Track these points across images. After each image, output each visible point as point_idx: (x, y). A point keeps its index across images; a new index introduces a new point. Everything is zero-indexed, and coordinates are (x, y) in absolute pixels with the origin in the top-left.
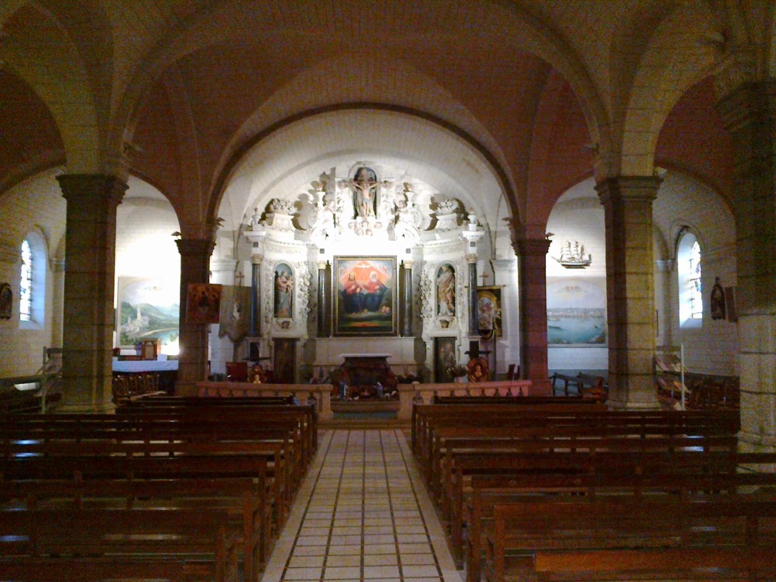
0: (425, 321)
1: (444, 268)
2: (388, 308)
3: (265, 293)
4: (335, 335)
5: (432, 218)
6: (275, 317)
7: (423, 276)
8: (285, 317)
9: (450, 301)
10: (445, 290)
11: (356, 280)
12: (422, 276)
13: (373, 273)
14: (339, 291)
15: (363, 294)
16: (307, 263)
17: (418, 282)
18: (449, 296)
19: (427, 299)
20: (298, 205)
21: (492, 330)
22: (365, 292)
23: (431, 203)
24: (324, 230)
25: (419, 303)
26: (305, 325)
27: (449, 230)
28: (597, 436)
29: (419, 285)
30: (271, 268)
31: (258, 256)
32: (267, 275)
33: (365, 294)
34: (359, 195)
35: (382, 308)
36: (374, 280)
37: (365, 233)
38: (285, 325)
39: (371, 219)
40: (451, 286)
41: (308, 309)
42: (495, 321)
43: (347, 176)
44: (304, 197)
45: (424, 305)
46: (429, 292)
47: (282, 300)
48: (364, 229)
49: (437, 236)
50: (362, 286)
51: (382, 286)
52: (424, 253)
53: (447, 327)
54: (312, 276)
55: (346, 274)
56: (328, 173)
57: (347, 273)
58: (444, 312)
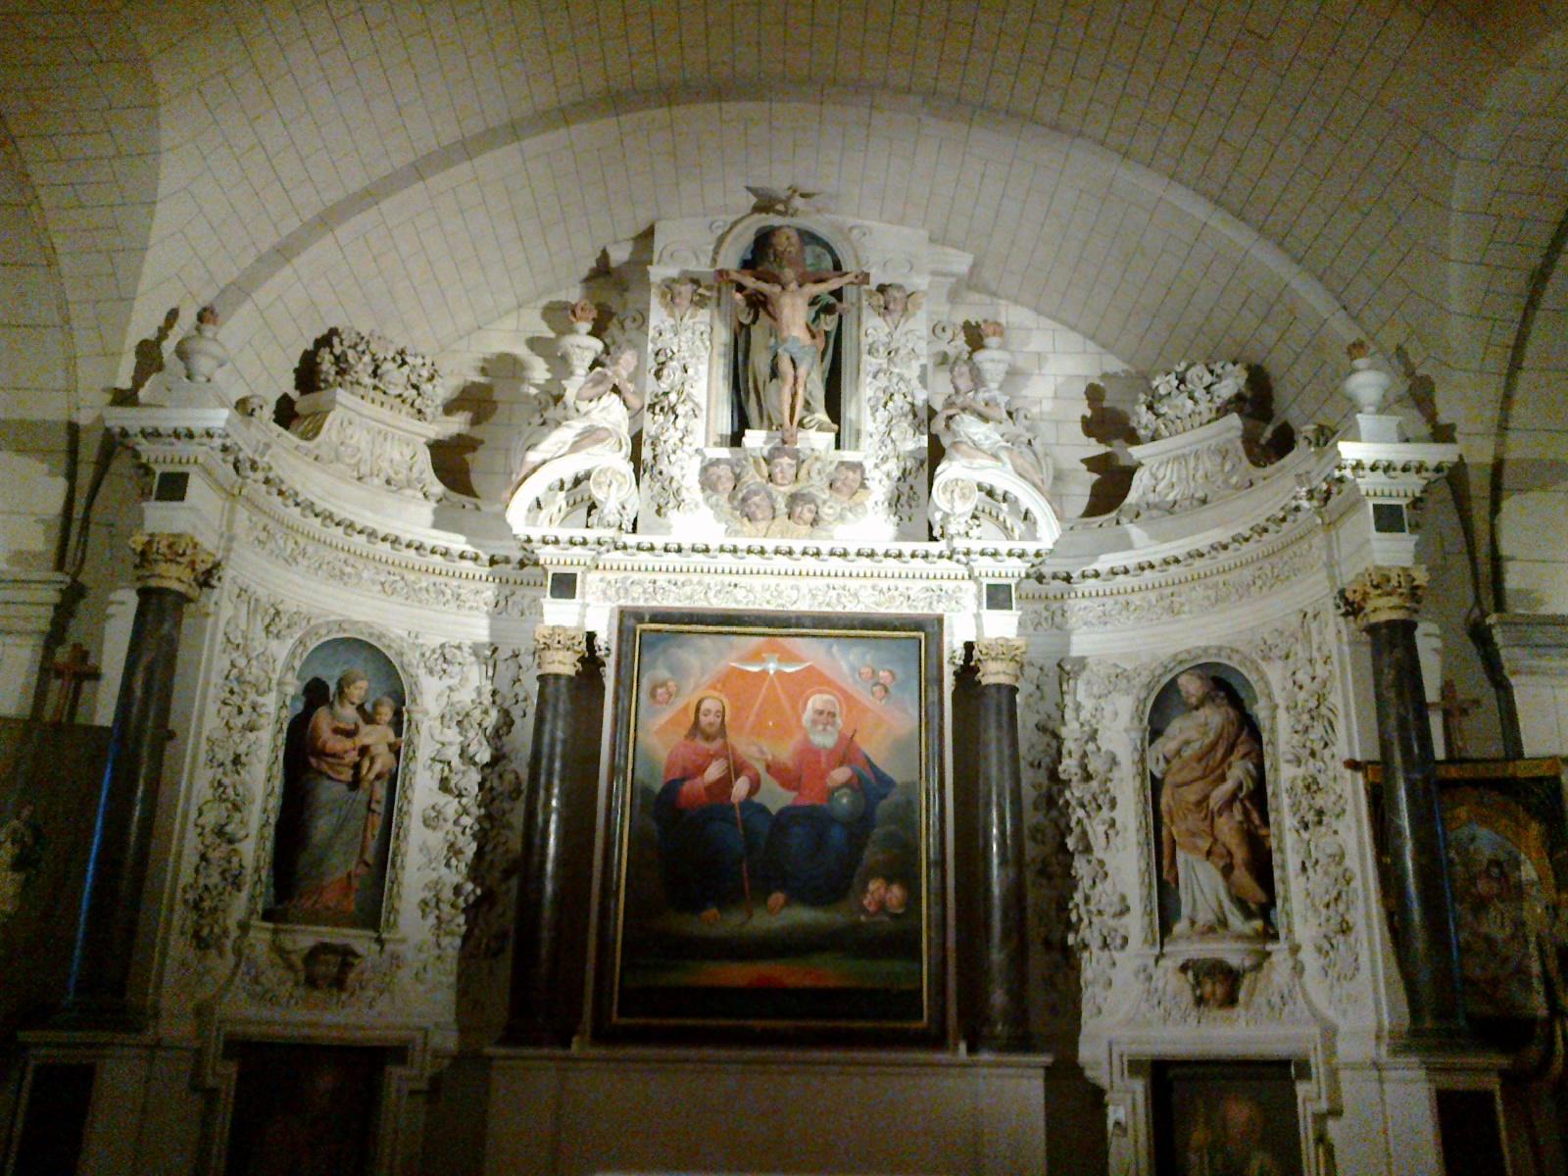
0: (1092, 967)
1: (1191, 686)
2: (896, 893)
3: (204, 778)
4: (605, 1035)
5: (1096, 477)
6: (267, 916)
7: (1070, 731)
8: (337, 919)
9: (1240, 855)
10: (1206, 797)
11: (732, 738)
12: (1064, 732)
13: (816, 701)
14: (641, 792)
15: (762, 809)
16: (490, 655)
17: (1046, 761)
18: (1228, 829)
19: (1098, 853)
20: (475, 401)
21: (1549, 1023)
22: (776, 797)
23: (1088, 413)
24: (577, 482)
25: (1056, 869)
26: (446, 974)
27: (1204, 501)
28: (94, 876)
29: (1053, 775)
30: (281, 650)
31: (177, 549)
32: (237, 683)
33: (774, 809)
34: (758, 334)
35: (864, 889)
36: (825, 740)
37: (781, 506)
38: (329, 966)
39: (817, 440)
40: (1238, 771)
41: (469, 886)
42: (1553, 964)
43: (706, 260)
44: (507, 367)
45: (1085, 884)
46: (1105, 813)
47: (322, 826)
48: (781, 492)
49: (1135, 531)
50: (761, 768)
51: (868, 774)
52: (1073, 621)
53: (1230, 1000)
54: (507, 721)
55: (679, 703)
56: (619, 255)
57: (688, 698)
58: (1205, 916)
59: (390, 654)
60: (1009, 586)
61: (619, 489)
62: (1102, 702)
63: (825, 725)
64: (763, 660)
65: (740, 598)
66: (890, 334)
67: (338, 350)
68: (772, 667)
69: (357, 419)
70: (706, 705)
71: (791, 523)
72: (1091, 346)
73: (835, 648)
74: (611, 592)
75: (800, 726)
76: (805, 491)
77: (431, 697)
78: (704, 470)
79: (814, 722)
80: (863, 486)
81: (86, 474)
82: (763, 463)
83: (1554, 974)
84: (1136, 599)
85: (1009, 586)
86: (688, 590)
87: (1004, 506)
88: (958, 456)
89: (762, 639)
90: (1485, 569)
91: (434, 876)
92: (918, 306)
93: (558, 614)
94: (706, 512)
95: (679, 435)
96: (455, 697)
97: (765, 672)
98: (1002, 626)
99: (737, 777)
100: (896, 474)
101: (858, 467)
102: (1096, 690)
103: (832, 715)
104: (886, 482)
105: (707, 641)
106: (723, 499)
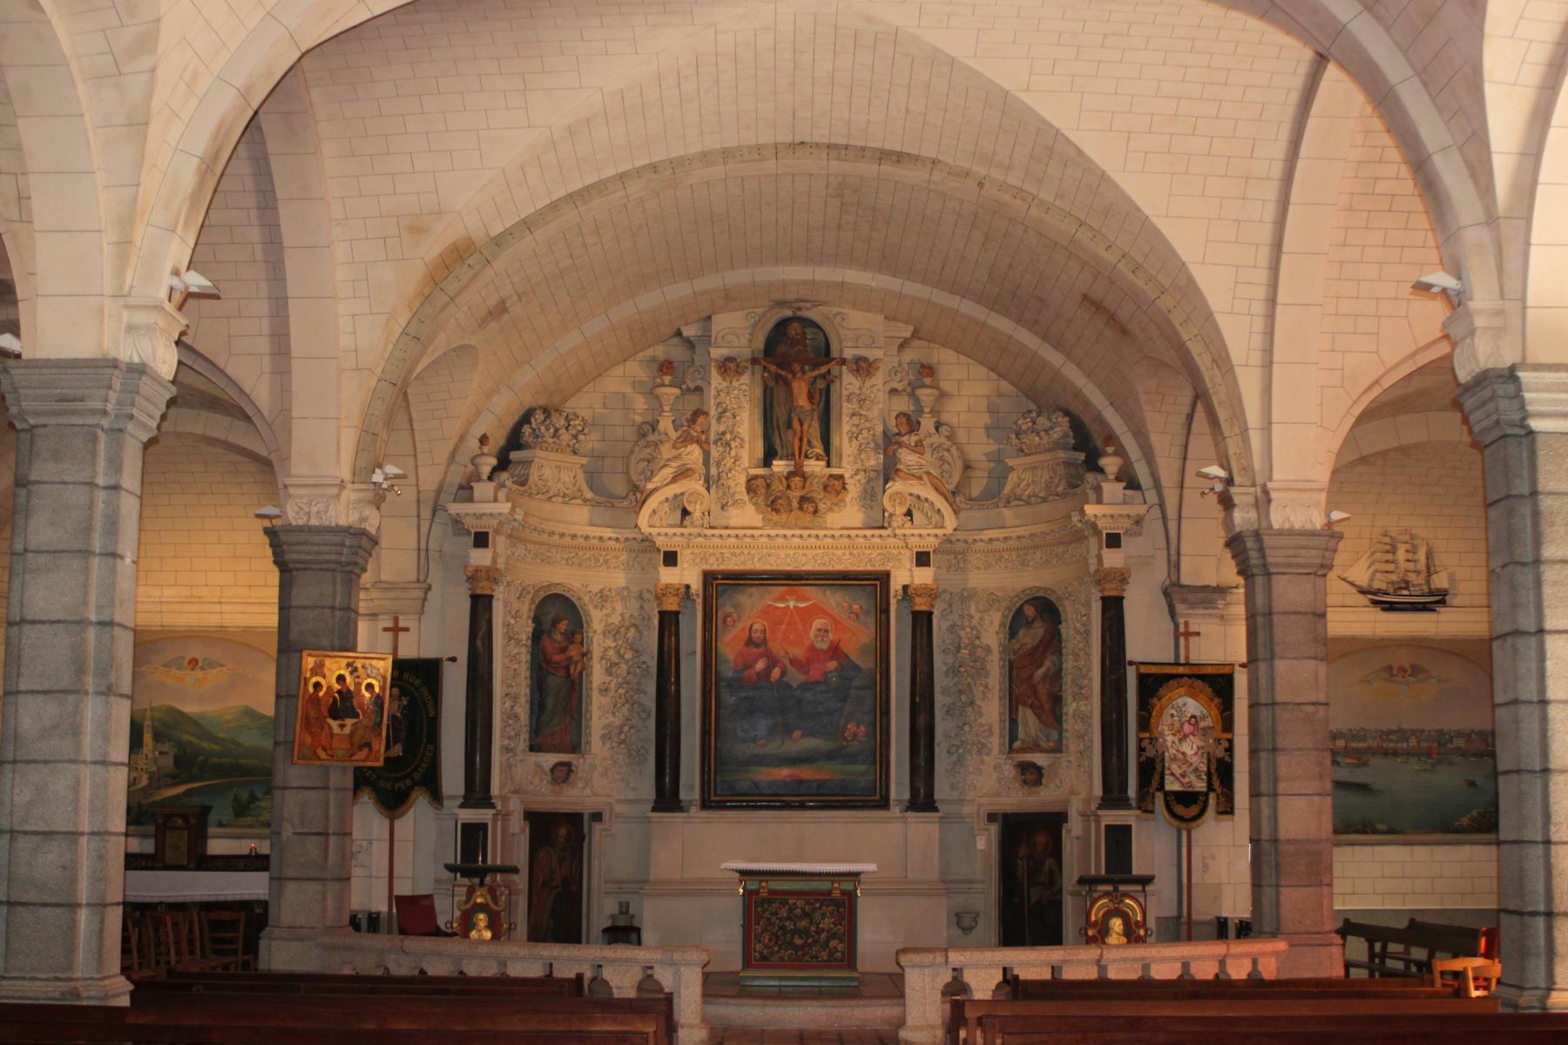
1: (1030, 611)
13: (818, 623)
37: (795, 504)
39: (814, 466)
42: (1213, 767)
43: (744, 341)
48: (795, 495)
50: (787, 662)
59: (574, 600)
60: (929, 553)
61: (701, 504)
62: (984, 614)
63: (822, 637)
64: (786, 600)
65: (772, 562)
66: (860, 388)
67: (534, 426)
68: (792, 604)
69: (545, 463)
70: (755, 627)
71: (800, 513)
72: (993, 376)
73: (828, 592)
74: (698, 561)
75: (809, 638)
76: (809, 496)
77: (597, 620)
78: (749, 481)
79: (817, 636)
80: (844, 488)
81: (424, 529)
82: (784, 480)
83: (1213, 771)
84: (1006, 555)
85: (929, 553)
86: (742, 558)
87: (926, 505)
88: (897, 479)
89: (784, 588)
90: (1174, 558)
91: (607, 722)
92: (877, 369)
93: (669, 576)
94: (750, 508)
95: (733, 460)
96: (610, 620)
97: (788, 607)
98: (924, 576)
99: (774, 667)
100: (863, 481)
101: (841, 477)
102: (981, 608)
103: (826, 631)
104: (858, 484)
105: (754, 589)
106: (761, 499)
